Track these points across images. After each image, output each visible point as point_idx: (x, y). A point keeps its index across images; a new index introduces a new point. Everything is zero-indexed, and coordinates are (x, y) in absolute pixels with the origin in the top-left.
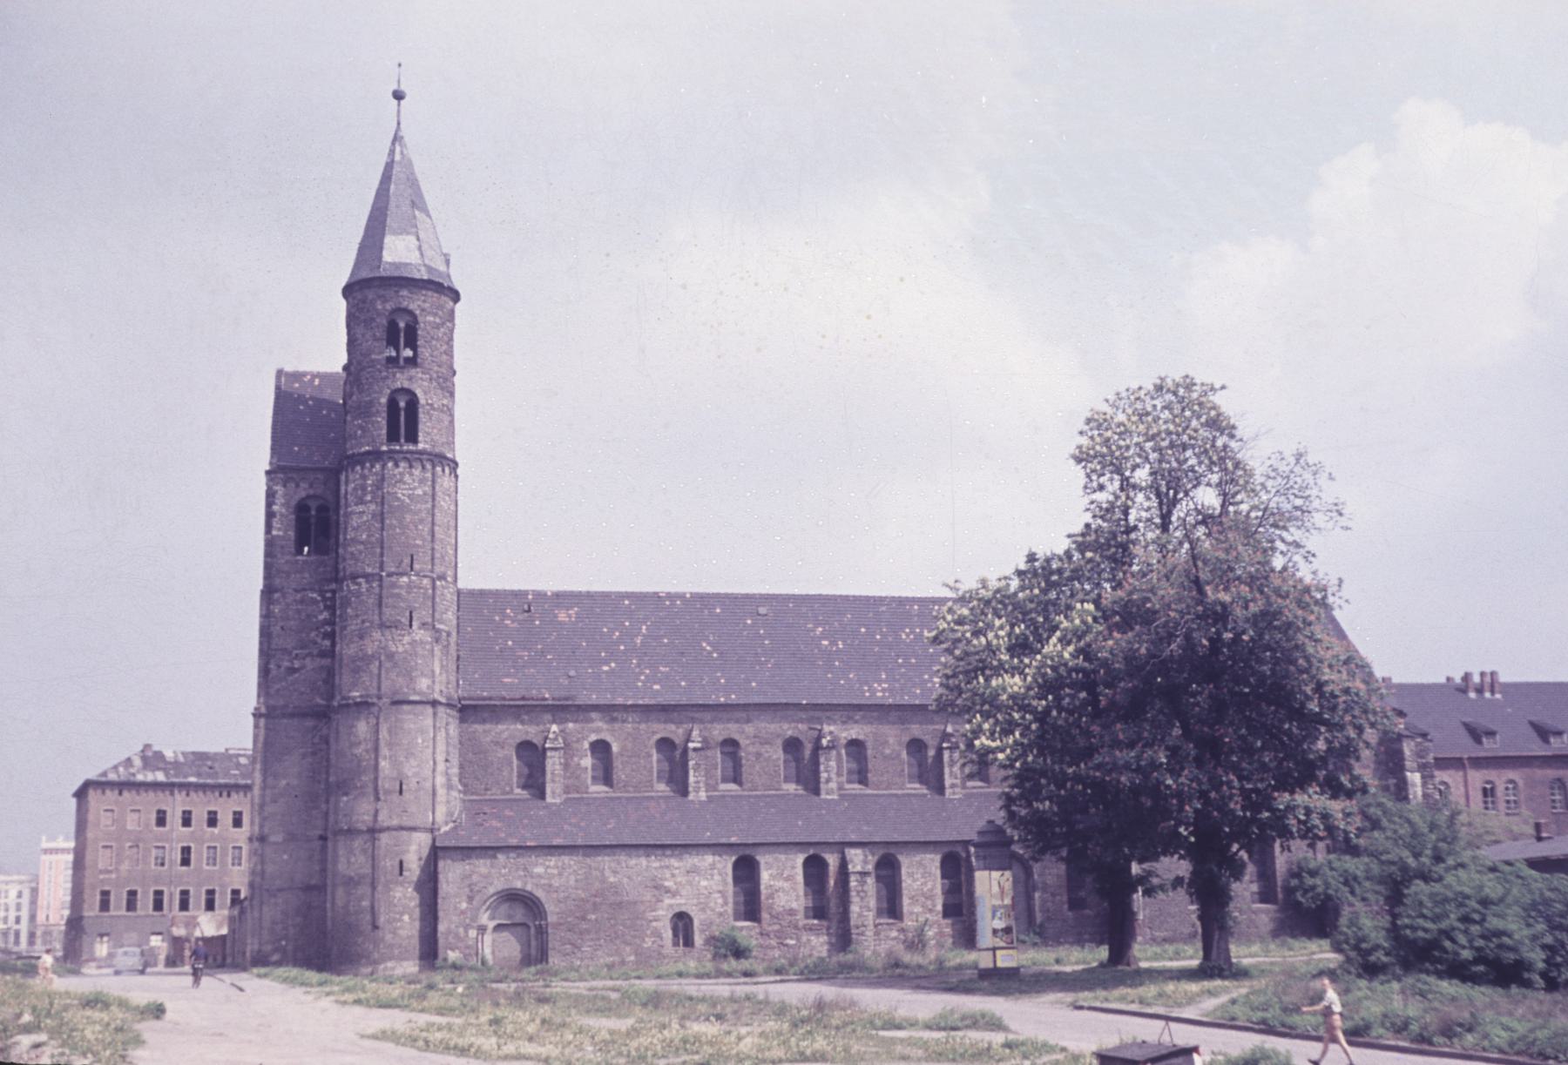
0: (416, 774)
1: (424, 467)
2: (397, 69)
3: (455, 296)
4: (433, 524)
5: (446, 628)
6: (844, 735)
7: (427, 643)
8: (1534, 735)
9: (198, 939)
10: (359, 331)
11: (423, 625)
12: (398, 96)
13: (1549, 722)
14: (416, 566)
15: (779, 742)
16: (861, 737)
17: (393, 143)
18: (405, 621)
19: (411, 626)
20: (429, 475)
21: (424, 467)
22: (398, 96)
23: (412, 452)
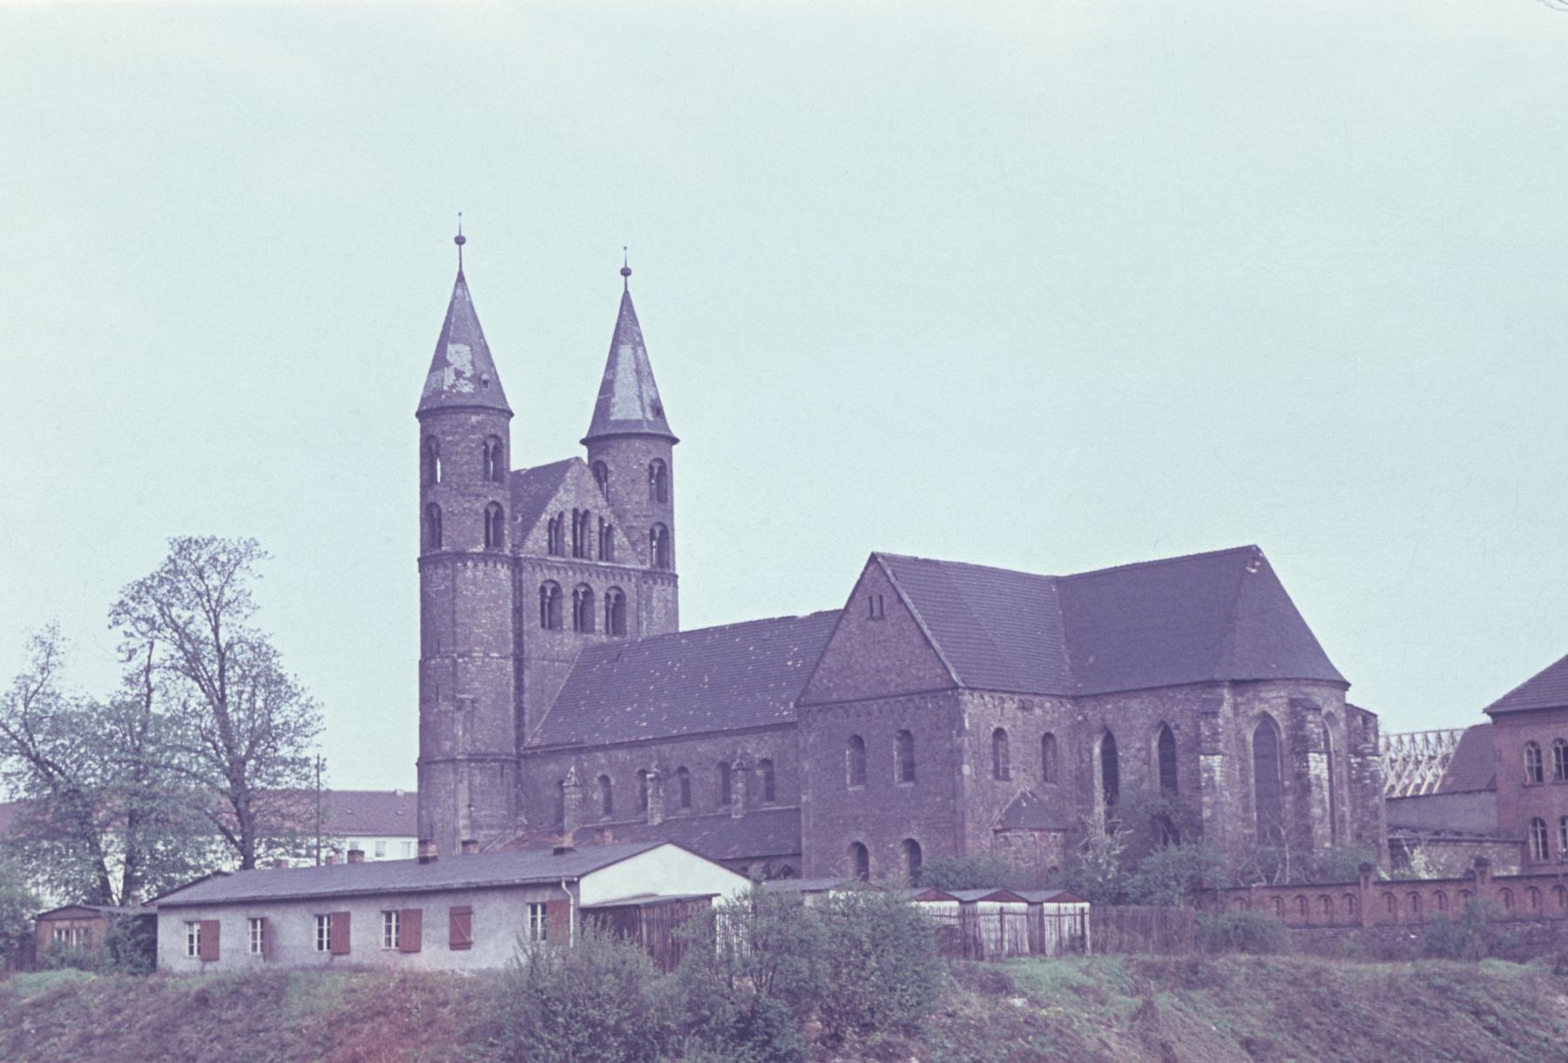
0: (442, 820)
1: (445, 566)
2: (458, 218)
3: (511, 414)
4: (454, 612)
5: (471, 697)
6: (757, 756)
7: (450, 711)
8: (455, 277)
9: (1304, 717)
10: (1308, 638)
11: (446, 698)
12: (460, 241)
13: (301, 892)
14: (442, 649)
15: (713, 767)
16: (769, 757)
17: (616, 342)
18: (433, 696)
19: (437, 700)
20: (449, 572)
21: (445, 566)
22: (460, 241)
23: (438, 555)
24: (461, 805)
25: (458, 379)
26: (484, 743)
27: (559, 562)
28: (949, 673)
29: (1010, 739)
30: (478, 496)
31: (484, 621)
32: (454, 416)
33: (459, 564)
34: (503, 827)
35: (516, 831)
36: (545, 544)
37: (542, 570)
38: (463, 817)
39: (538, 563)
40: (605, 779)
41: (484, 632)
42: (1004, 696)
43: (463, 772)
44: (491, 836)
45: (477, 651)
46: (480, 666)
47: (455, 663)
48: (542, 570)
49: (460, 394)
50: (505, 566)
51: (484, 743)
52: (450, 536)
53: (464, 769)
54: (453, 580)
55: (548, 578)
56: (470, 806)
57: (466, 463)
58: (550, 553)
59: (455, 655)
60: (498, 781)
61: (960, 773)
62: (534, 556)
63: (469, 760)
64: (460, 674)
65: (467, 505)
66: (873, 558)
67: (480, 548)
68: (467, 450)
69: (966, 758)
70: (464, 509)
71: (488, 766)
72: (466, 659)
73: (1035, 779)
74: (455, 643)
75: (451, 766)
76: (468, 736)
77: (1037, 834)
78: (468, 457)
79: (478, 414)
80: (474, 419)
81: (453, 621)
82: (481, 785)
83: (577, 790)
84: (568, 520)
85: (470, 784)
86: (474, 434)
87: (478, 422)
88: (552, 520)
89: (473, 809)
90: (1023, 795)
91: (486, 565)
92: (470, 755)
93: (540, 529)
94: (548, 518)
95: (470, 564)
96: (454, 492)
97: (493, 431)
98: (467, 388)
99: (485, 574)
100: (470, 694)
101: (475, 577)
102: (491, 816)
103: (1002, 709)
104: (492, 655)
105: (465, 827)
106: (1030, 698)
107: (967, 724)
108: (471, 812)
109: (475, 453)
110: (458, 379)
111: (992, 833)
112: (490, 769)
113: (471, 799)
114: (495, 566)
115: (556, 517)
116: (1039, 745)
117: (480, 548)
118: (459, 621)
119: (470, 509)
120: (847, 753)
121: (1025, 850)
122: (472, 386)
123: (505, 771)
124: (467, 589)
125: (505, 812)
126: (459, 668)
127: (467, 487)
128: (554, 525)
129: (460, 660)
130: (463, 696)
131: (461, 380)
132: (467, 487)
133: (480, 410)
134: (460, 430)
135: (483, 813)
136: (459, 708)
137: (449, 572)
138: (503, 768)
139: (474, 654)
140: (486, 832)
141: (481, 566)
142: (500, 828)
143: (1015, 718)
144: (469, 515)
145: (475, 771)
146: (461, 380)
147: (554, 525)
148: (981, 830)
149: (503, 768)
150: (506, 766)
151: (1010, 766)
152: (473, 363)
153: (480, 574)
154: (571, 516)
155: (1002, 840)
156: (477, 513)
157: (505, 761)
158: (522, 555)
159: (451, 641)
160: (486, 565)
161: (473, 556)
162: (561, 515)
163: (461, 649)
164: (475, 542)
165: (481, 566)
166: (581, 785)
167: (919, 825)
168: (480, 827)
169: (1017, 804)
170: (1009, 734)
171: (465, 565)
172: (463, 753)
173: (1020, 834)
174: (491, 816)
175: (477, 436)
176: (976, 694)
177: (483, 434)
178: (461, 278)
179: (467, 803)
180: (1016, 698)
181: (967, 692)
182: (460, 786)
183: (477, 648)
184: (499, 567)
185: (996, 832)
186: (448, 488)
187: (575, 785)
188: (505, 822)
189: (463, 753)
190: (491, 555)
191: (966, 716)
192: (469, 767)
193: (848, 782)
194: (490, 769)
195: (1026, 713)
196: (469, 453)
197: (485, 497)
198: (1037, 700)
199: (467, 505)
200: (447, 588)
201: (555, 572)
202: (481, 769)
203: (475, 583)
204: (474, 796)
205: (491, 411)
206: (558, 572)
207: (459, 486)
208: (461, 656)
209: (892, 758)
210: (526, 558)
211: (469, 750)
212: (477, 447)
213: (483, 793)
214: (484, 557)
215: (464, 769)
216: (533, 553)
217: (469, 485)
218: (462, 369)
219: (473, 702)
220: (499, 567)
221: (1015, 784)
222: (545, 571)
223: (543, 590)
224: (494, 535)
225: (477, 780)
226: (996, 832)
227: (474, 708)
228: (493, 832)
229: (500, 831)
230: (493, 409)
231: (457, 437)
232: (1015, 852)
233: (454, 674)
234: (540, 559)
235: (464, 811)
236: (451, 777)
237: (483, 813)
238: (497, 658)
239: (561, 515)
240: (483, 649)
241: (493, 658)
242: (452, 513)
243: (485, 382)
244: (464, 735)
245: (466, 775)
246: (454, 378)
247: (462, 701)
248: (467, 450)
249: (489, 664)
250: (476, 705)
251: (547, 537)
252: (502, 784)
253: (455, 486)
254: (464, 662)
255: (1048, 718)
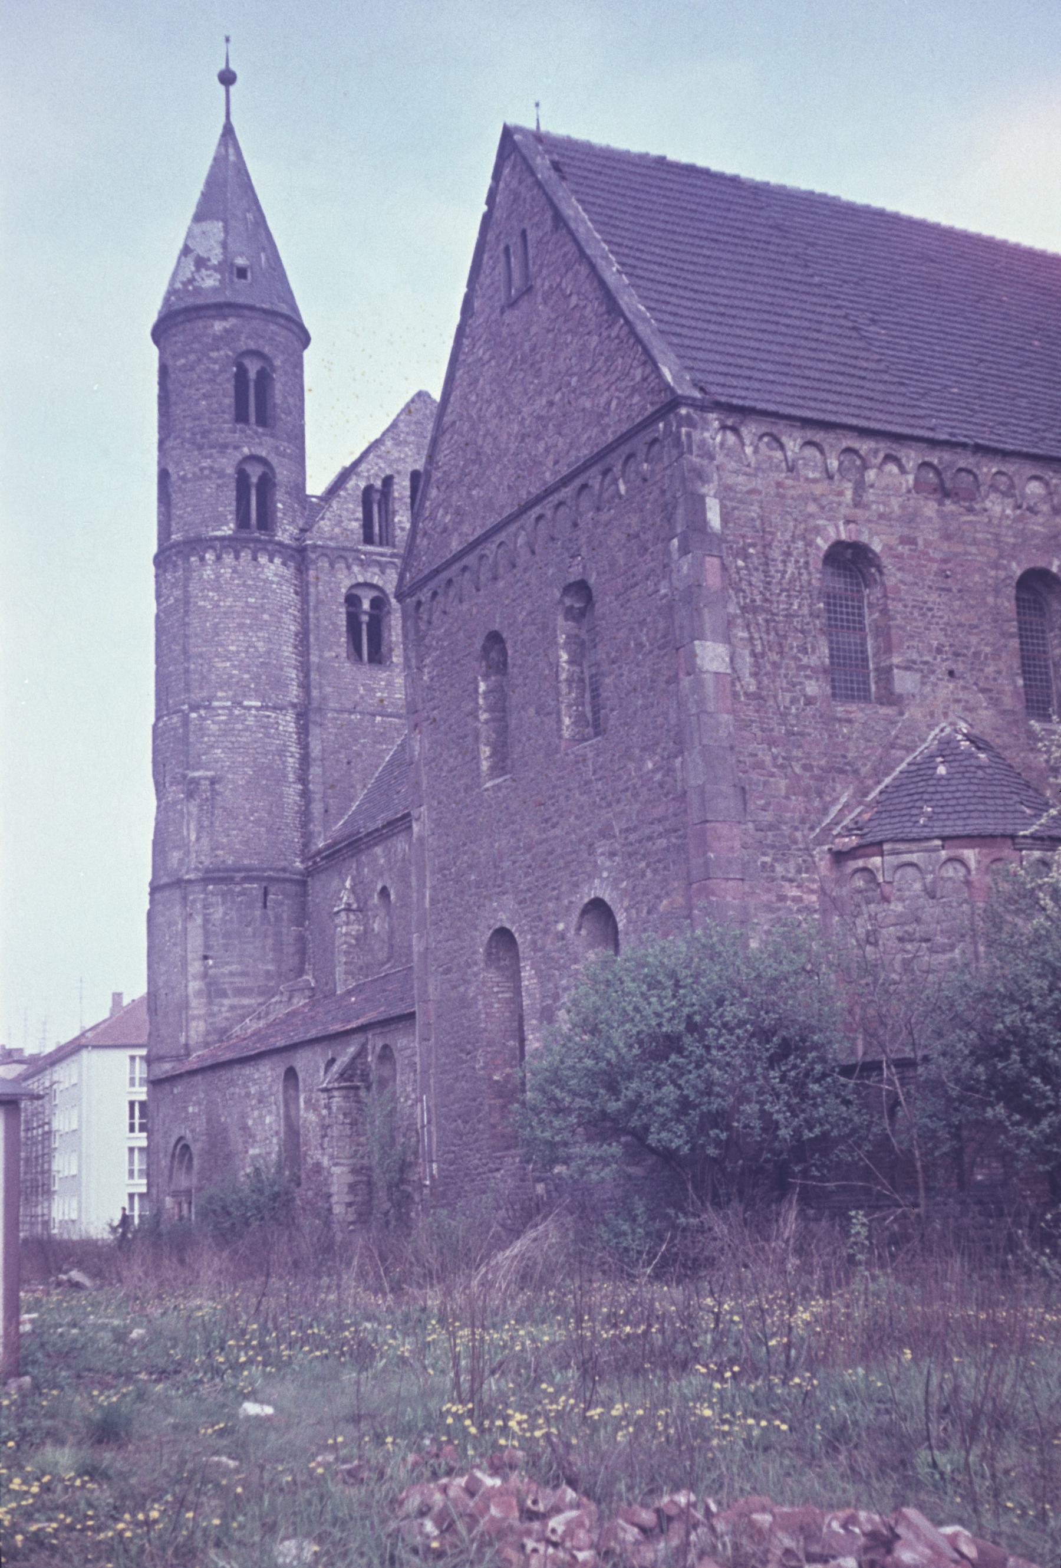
5: (210, 774)
8: (219, 130)
12: (227, 78)
22: (227, 78)
24: (190, 956)
25: (198, 270)
26: (232, 851)
27: (382, 555)
28: (650, 361)
29: (893, 577)
30: (223, 447)
31: (233, 648)
32: (188, 326)
33: (192, 559)
34: (267, 993)
35: (290, 999)
36: (355, 525)
37: (349, 567)
38: (195, 978)
39: (340, 555)
40: (384, 892)
41: (234, 667)
42: (865, 446)
43: (194, 901)
44: (243, 1007)
45: (221, 699)
46: (226, 723)
47: (186, 722)
48: (349, 567)
49: (198, 291)
50: (277, 560)
51: (232, 851)
52: (181, 517)
53: (196, 895)
54: (185, 587)
55: (361, 579)
56: (206, 958)
57: (205, 396)
58: (368, 539)
59: (186, 707)
60: (258, 913)
61: (692, 670)
62: (332, 544)
63: (206, 880)
64: (192, 739)
65: (206, 463)
66: (508, 133)
67: (228, 529)
68: (205, 376)
69: (709, 620)
70: (202, 469)
71: (238, 889)
72: (202, 712)
73: (995, 702)
74: (188, 689)
75: (177, 894)
76: (205, 841)
77: (970, 855)
78: (208, 387)
79: (225, 318)
80: (218, 326)
81: (185, 651)
82: (224, 922)
83: (352, 917)
84: (402, 488)
85: (206, 921)
86: (218, 350)
87: (226, 330)
88: (368, 490)
89: (211, 962)
90: (946, 749)
91: (237, 557)
92: (207, 871)
93: (346, 501)
94: (362, 485)
95: (209, 556)
96: (187, 446)
97: (252, 345)
98: (210, 281)
99: (235, 571)
100: (207, 769)
101: (218, 576)
102: (244, 974)
103: (860, 487)
104: (246, 703)
105: (198, 994)
106: (965, 460)
107: (714, 518)
108: (207, 968)
109: (219, 380)
110: (198, 270)
111: (824, 865)
112: (240, 894)
113: (207, 947)
114: (255, 559)
115: (378, 484)
116: (1008, 605)
117: (228, 529)
118: (194, 651)
119: (211, 469)
120: (482, 687)
121: (931, 910)
122: (219, 276)
123: (271, 897)
124: (205, 598)
125: (271, 967)
126: (192, 728)
127: (205, 433)
128: (376, 497)
129: (194, 715)
130: (197, 774)
131: (203, 271)
132: (205, 433)
133: (226, 311)
134: (196, 346)
135: (226, 970)
136: (190, 795)
137: (179, 573)
138: (266, 893)
139: (216, 704)
140: (236, 1001)
141: (228, 559)
142: (261, 993)
143: (911, 518)
144: (208, 478)
145: (213, 899)
146: (203, 271)
147: (376, 497)
148: (783, 853)
149: (266, 893)
150: (272, 889)
151: (896, 660)
152: (224, 245)
153: (227, 572)
154: (407, 483)
155: (860, 883)
156: (221, 474)
157: (270, 879)
158: (309, 542)
159: (182, 685)
160: (237, 557)
161: (210, 543)
162: (388, 481)
163: (197, 696)
164: (220, 521)
165: (228, 559)
166: (360, 910)
167: (612, 854)
168: (224, 994)
169: (922, 770)
170: (886, 561)
171: (202, 559)
172: (196, 869)
173: (914, 857)
174: (244, 974)
175: (226, 352)
176: (750, 430)
177: (233, 350)
178: (228, 131)
179: (200, 954)
180: (911, 457)
181: (714, 419)
182: (190, 926)
183: (220, 694)
184: (263, 560)
185: (839, 857)
186: (179, 441)
187: (348, 909)
188: (272, 984)
189: (196, 869)
190: (247, 540)
191: (709, 490)
192: (204, 891)
193: (485, 765)
194: (240, 894)
195: (950, 506)
196: (211, 381)
197: (237, 448)
198: (989, 469)
199: (206, 463)
200: (177, 600)
201: (376, 570)
202: (224, 895)
203: (218, 589)
204: (213, 942)
205: (247, 313)
206: (383, 572)
207: (194, 434)
208: (194, 708)
209: (555, 666)
210: (315, 547)
211: (207, 862)
212: (222, 371)
213: (227, 935)
214: (232, 544)
215: (196, 895)
216: (331, 539)
217: (209, 431)
218: (205, 255)
219: (213, 781)
220: (263, 560)
221: (914, 712)
222: (356, 569)
223: (352, 600)
224: (258, 510)
225: (218, 913)
226: (839, 857)
227: (215, 793)
228: (246, 1001)
229: (261, 1000)
230: (252, 308)
231: (192, 357)
232: (900, 921)
233: (185, 740)
234: (344, 549)
235: (195, 967)
236: (177, 909)
237: (226, 970)
238: (257, 709)
239: (388, 481)
240: (231, 693)
241: (249, 708)
242: (183, 479)
243: (242, 273)
244: (198, 839)
245: (199, 905)
246: (193, 268)
247: (195, 781)
248: (205, 376)
249: (241, 719)
250: (217, 786)
251: (360, 515)
252: (265, 918)
253: (188, 435)
254: (200, 716)
255: (1037, 525)
